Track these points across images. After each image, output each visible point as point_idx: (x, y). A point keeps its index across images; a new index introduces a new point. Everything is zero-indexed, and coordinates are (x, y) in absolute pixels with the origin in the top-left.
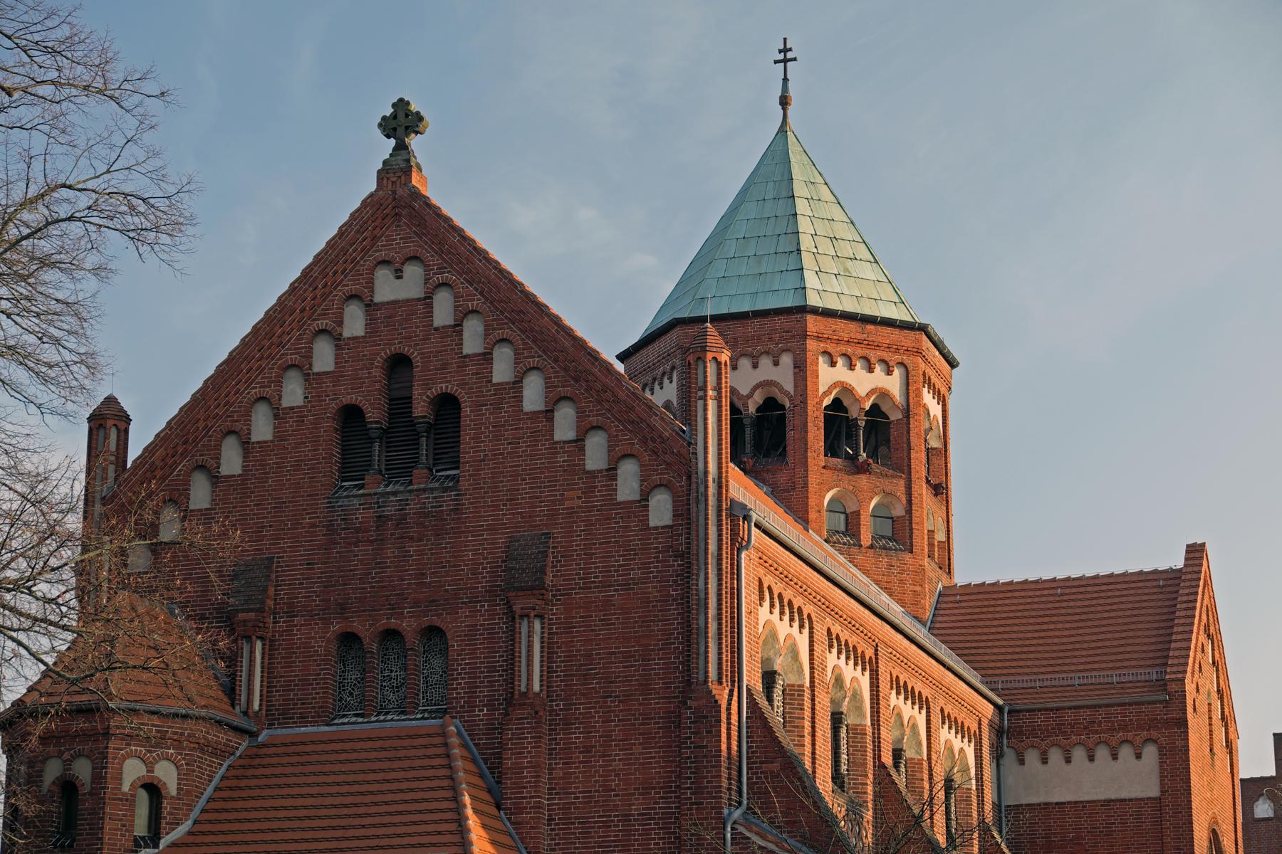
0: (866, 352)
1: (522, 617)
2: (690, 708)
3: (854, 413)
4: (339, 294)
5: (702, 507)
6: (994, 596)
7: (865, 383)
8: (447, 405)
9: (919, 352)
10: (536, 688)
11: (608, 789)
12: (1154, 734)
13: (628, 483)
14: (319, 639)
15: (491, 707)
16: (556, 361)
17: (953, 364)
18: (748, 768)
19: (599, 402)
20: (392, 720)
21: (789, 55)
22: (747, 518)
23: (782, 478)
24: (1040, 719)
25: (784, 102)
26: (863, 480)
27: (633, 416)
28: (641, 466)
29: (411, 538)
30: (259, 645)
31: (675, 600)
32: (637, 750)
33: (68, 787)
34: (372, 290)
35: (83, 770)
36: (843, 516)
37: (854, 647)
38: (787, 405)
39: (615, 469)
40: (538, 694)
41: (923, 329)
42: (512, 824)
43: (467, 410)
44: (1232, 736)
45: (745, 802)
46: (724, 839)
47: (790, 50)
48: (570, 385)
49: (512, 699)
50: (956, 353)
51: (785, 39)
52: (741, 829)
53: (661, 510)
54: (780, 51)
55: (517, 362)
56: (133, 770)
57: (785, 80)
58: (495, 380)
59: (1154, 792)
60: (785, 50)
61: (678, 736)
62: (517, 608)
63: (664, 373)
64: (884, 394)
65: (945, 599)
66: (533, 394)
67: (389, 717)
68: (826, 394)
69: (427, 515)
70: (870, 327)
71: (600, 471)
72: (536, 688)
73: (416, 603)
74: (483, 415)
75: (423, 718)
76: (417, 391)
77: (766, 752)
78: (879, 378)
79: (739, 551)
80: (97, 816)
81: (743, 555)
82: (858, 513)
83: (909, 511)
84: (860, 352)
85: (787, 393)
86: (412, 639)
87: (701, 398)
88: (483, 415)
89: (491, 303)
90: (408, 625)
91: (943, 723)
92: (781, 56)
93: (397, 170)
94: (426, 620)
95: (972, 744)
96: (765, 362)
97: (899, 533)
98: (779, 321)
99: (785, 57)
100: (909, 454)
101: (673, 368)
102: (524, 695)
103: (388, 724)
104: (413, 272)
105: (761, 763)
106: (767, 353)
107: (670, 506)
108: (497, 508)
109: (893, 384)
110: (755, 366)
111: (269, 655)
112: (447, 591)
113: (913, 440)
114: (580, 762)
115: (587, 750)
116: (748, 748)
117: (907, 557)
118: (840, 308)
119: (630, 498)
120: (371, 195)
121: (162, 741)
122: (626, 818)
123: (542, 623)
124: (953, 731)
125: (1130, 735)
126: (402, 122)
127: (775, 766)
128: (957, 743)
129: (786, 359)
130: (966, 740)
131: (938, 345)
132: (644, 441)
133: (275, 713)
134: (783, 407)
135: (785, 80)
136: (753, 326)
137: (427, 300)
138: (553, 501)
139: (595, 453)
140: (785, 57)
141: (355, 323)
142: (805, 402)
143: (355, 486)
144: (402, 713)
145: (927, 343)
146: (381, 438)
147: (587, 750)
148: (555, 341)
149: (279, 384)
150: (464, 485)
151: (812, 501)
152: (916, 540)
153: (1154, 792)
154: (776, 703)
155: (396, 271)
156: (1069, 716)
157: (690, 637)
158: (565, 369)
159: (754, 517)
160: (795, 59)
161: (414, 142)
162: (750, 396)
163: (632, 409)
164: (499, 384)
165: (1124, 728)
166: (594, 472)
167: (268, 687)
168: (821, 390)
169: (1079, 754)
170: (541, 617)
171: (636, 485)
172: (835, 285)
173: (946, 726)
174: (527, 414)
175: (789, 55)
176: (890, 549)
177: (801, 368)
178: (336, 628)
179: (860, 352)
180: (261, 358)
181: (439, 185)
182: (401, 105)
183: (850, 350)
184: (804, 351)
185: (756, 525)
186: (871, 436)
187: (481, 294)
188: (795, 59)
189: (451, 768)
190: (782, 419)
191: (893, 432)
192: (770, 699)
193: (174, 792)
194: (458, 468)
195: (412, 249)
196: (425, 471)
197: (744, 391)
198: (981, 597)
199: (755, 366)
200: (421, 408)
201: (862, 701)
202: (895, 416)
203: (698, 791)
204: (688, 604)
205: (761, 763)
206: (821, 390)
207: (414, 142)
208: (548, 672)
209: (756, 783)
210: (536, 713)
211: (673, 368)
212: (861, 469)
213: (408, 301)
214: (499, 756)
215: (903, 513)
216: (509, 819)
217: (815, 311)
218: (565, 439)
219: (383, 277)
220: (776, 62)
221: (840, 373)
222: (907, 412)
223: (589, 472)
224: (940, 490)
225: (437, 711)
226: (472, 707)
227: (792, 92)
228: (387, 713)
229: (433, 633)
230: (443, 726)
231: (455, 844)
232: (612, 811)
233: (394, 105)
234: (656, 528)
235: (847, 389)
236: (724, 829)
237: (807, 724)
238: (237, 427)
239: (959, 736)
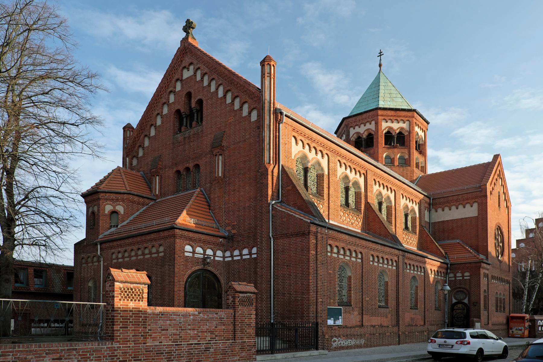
0: (397, 118)
3: (394, 134)
4: (174, 80)
7: (396, 126)
9: (413, 117)
10: (220, 175)
11: (239, 201)
12: (476, 200)
14: (170, 173)
19: (237, 88)
22: (281, 113)
23: (372, 151)
24: (442, 200)
25: (380, 65)
26: (396, 150)
27: (245, 89)
30: (157, 178)
32: (247, 188)
33: (93, 213)
35: (96, 209)
41: (415, 111)
43: (204, 102)
44: (508, 204)
50: (428, 119)
52: (275, 206)
53: (254, 116)
56: (108, 208)
59: (476, 215)
60: (381, 52)
64: (402, 128)
68: (384, 130)
72: (220, 175)
73: (193, 159)
78: (401, 125)
79: (279, 124)
80: (98, 219)
81: (281, 125)
82: (394, 158)
83: (410, 157)
84: (395, 118)
90: (191, 165)
94: (195, 163)
96: (368, 124)
97: (406, 162)
98: (371, 113)
99: (381, 54)
106: (368, 122)
108: (212, 127)
109: (405, 126)
111: (160, 180)
113: (411, 139)
117: (409, 168)
121: (117, 200)
125: (469, 201)
126: (188, 27)
127: (290, 188)
129: (373, 122)
131: (421, 116)
133: (162, 195)
136: (364, 116)
140: (381, 54)
141: (179, 87)
142: (378, 132)
145: (415, 114)
147: (234, 191)
149: (162, 109)
151: (380, 155)
152: (412, 164)
153: (476, 215)
154: (383, 212)
156: (451, 198)
159: (285, 113)
163: (244, 87)
165: (467, 199)
167: (160, 188)
169: (453, 208)
177: (377, 124)
178: (175, 170)
179: (395, 118)
181: (199, 41)
183: (392, 118)
184: (378, 119)
185: (286, 116)
186: (397, 140)
190: (373, 137)
191: (406, 138)
192: (380, 210)
193: (123, 213)
195: (190, 61)
197: (362, 133)
202: (406, 134)
212: (394, 147)
217: (380, 109)
221: (389, 124)
222: (409, 132)
227: (382, 62)
235: (390, 128)
238: (154, 123)
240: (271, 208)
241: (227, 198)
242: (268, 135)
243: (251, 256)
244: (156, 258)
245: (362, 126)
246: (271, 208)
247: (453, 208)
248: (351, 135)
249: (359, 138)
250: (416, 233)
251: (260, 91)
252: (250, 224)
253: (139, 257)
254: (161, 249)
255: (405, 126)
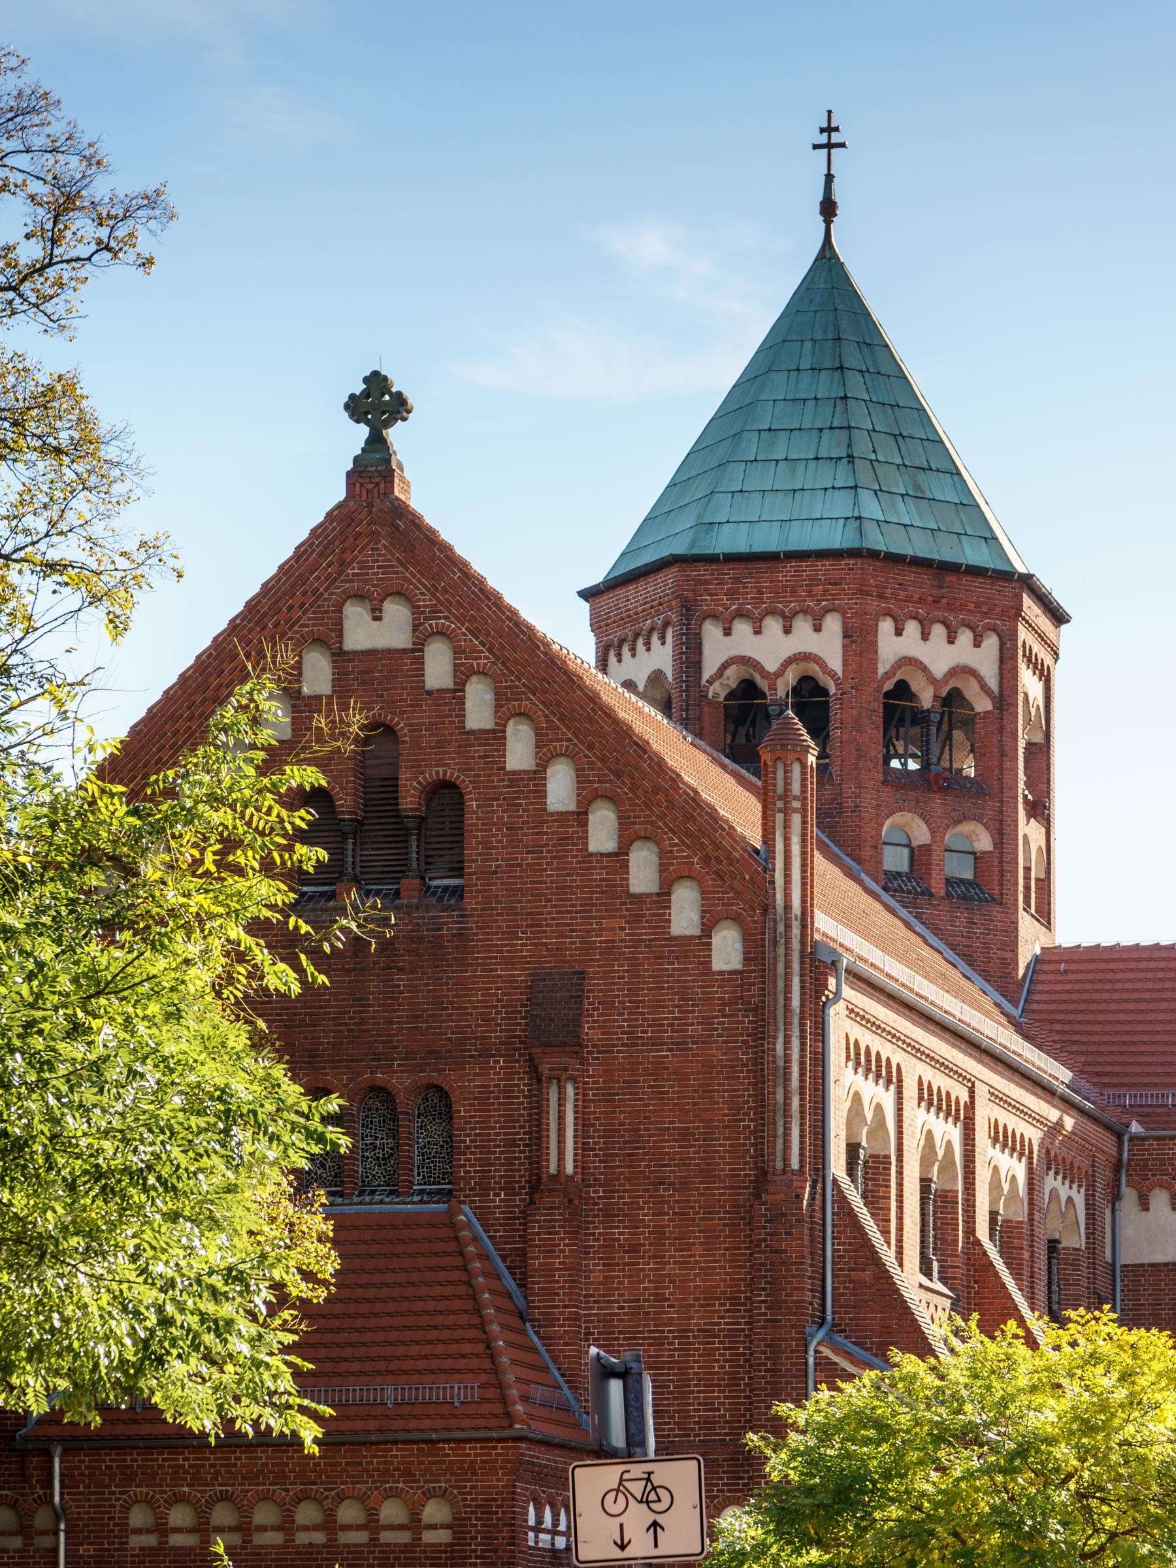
1: (550, 1079)
2: (766, 1203)
5: (781, 951)
6: (1112, 966)
8: (445, 792)
10: (569, 1168)
13: (685, 912)
15: (510, 1189)
16: (590, 747)
17: (1059, 617)
18: (834, 1276)
20: (381, 1202)
21: (836, 138)
25: (828, 209)
28: (703, 892)
29: (401, 969)
31: (746, 1065)
32: (698, 1250)
34: (340, 635)
36: (906, 851)
37: (948, 1094)
38: (832, 690)
39: (669, 894)
40: (572, 1177)
42: (540, 1338)
45: (829, 1318)
46: (806, 1364)
47: (837, 129)
48: (610, 781)
49: (538, 1184)
51: (830, 112)
53: (727, 950)
54: (822, 130)
55: (539, 746)
57: (829, 177)
58: (509, 767)
60: (829, 129)
61: (750, 1236)
62: (545, 1068)
63: (652, 630)
65: (1045, 967)
66: (560, 788)
67: (377, 1198)
68: (888, 675)
69: (421, 939)
70: (950, 579)
71: (649, 895)
72: (569, 1168)
74: (494, 812)
75: (421, 1202)
76: (404, 775)
77: (856, 1257)
85: (832, 674)
86: (406, 1102)
87: (780, 810)
88: (494, 812)
89: (503, 664)
91: (1049, 1169)
92: (823, 139)
93: (373, 472)
95: (1083, 1191)
96: (802, 626)
99: (829, 140)
100: (1001, 762)
101: (666, 624)
102: (554, 1178)
103: (377, 1208)
104: (396, 613)
105: (850, 1270)
106: (805, 611)
107: (739, 946)
110: (787, 631)
112: (450, 1039)
114: (625, 1264)
115: (634, 1249)
116: (834, 1251)
118: (909, 552)
119: (688, 933)
120: (339, 506)
122: (683, 1334)
123: (576, 1088)
124: (1060, 1178)
126: (378, 404)
127: (867, 1275)
128: (1064, 1191)
130: (1075, 1186)
132: (706, 860)
134: (825, 692)
135: (829, 177)
136: (787, 573)
137: (416, 652)
138: (588, 931)
139: (643, 871)
140: (829, 140)
143: (323, 894)
144: (392, 1193)
146: (355, 833)
147: (634, 1249)
148: (591, 721)
150: (472, 902)
155: (373, 610)
157: (763, 1115)
158: (603, 760)
160: (843, 145)
161: (395, 434)
162: (780, 673)
164: (515, 773)
166: (640, 895)
168: (881, 670)
170: (574, 1080)
171: (695, 916)
172: (905, 513)
173: (1052, 1173)
174: (552, 814)
175: (836, 138)
176: (972, 899)
180: (190, 719)
181: (431, 489)
182: (376, 382)
187: (490, 650)
188: (843, 145)
189: (466, 1270)
194: (461, 876)
196: (418, 881)
197: (771, 666)
198: (1093, 966)
199: (787, 631)
200: (410, 800)
201: (954, 1163)
202: (983, 705)
203: (775, 1305)
204: (762, 1072)
205: (850, 1270)
206: (881, 670)
207: (395, 434)
208: (582, 1148)
209: (843, 1294)
210: (570, 1201)
211: (666, 624)
213: (390, 651)
214: (523, 1253)
215: (990, 847)
216: (537, 1333)
218: (603, 850)
219: (355, 616)
220: (815, 147)
223: (634, 896)
224: (1040, 809)
225: (439, 1192)
226: (485, 1189)
227: (837, 196)
228: (372, 1193)
229: (438, 1102)
230: (451, 1213)
231: (485, 1371)
232: (666, 1325)
233: (366, 380)
234: (721, 973)
236: (806, 1352)
237: (893, 1204)
239: (1067, 1182)
240: (811, 1360)
241: (597, 1276)
242: (789, 1048)
243: (532, 1529)
244: (406, 1548)
245: (773, 625)
246: (811, 1360)
247: (938, 631)
248: (709, 668)
249: (748, 690)
250: (334, 892)
251: (761, 860)
252: (709, 1406)
253: (302, 1538)
254: (435, 1511)
255: (984, 659)
